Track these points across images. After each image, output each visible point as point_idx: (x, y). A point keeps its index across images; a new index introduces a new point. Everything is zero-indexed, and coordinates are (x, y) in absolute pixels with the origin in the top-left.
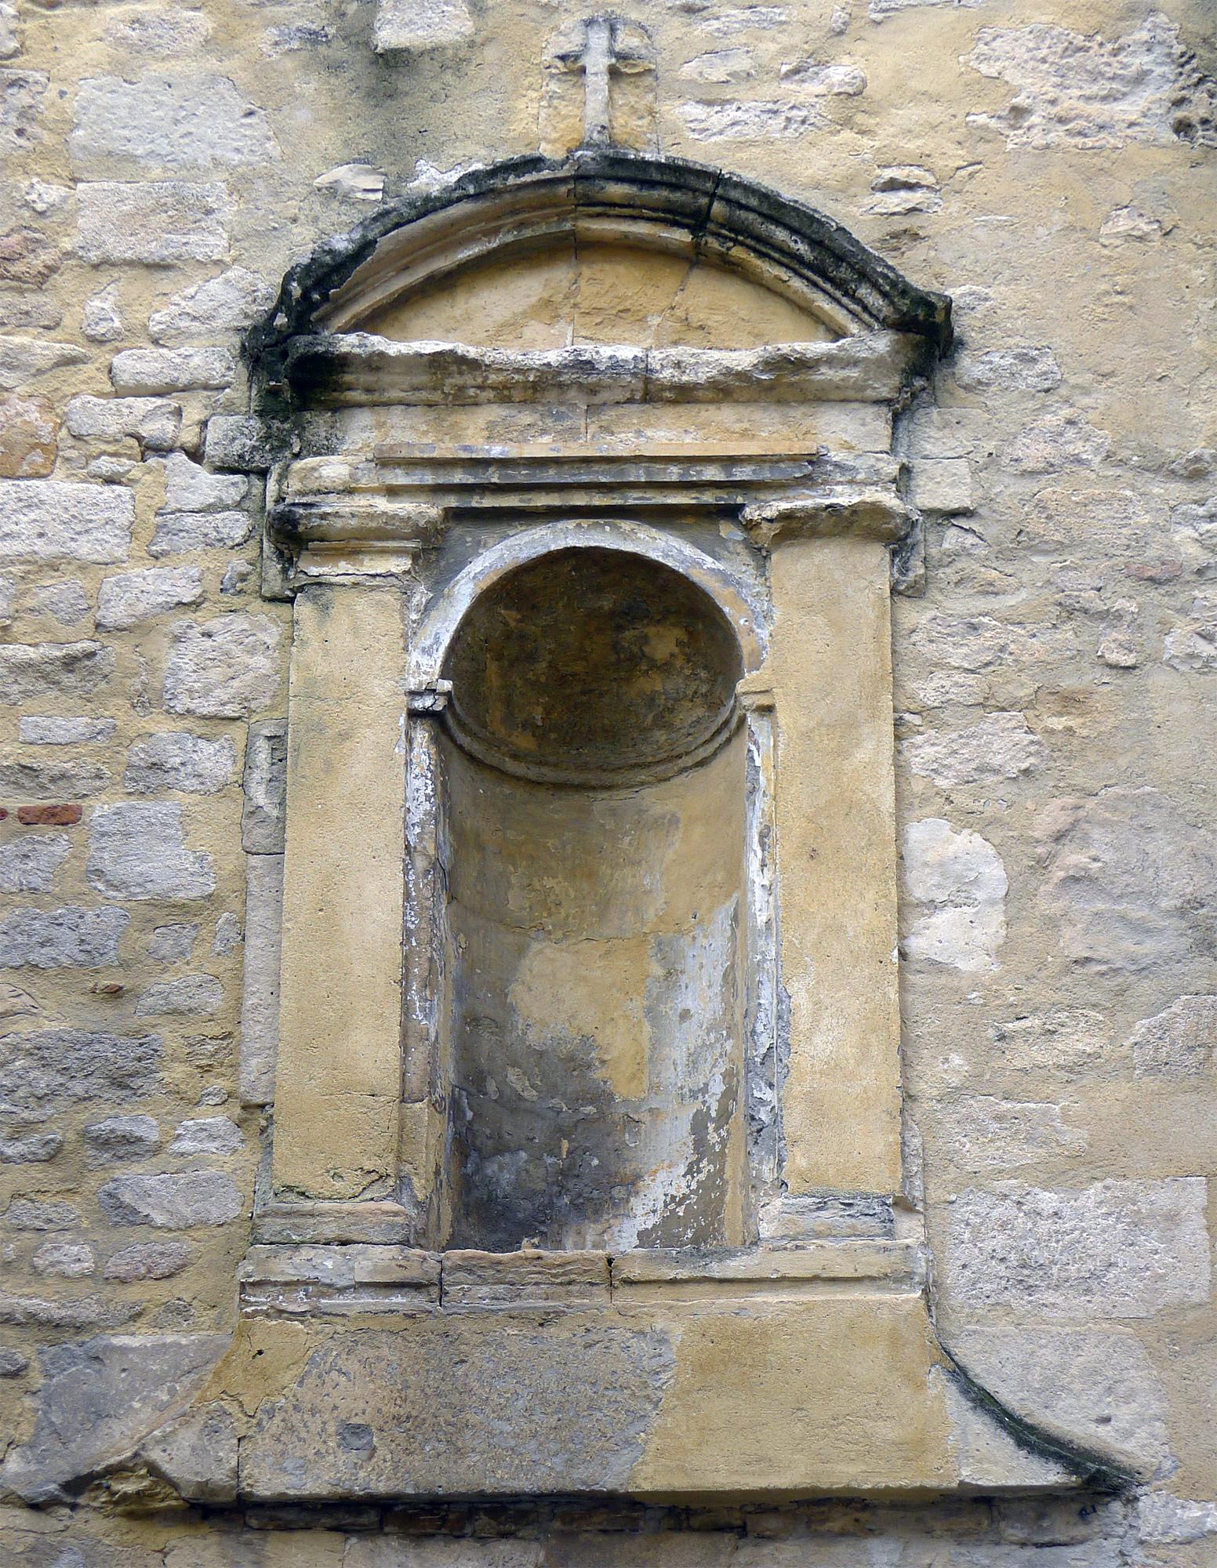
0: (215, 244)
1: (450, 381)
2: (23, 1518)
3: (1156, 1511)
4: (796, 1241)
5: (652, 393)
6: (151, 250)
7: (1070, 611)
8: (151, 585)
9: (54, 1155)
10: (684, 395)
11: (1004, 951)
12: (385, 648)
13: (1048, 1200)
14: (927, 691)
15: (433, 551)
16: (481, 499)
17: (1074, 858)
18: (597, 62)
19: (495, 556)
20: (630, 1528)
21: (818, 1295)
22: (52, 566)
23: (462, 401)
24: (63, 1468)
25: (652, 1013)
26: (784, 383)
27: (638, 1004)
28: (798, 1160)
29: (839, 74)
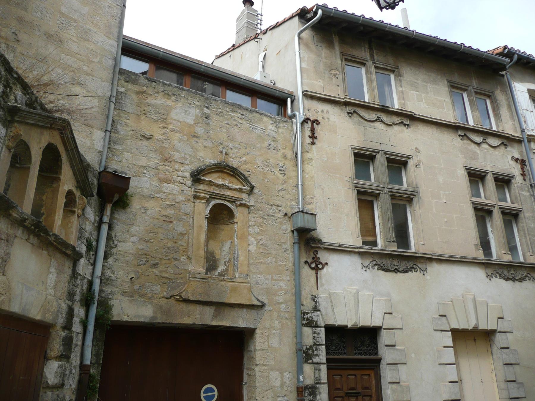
0: (188, 162)
1: (211, 183)
2: (165, 299)
3: (267, 308)
4: (240, 278)
5: (228, 188)
6: (181, 162)
7: (262, 217)
8: (181, 198)
9: (169, 259)
10: (231, 189)
11: (255, 250)
12: (203, 210)
13: (259, 276)
14: (251, 223)
15: (208, 201)
16: (213, 196)
17: (261, 242)
18: (224, 153)
19: (213, 202)
20: (243, 308)
21: (241, 284)
22: (171, 194)
23: (211, 185)
24: (171, 294)
25: (221, 250)
26: (240, 190)
27: (219, 248)
28: (239, 270)
29: (244, 159)
